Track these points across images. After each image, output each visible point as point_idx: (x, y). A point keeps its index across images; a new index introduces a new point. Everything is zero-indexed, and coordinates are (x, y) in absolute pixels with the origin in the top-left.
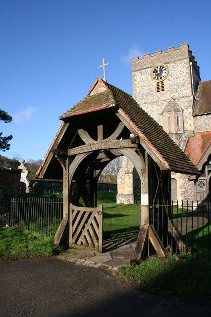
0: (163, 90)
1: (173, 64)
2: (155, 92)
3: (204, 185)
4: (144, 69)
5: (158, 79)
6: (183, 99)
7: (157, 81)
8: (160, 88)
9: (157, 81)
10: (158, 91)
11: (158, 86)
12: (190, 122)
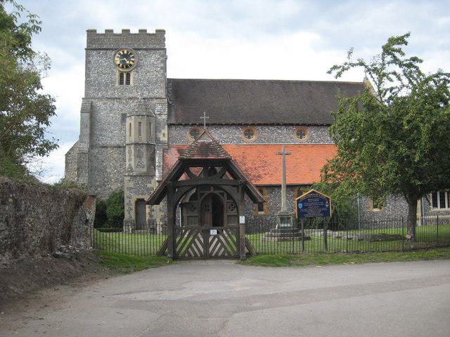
0: (128, 82)
1: (145, 52)
2: (117, 85)
3: (195, 208)
4: (104, 49)
5: (123, 67)
6: (155, 101)
7: (121, 70)
8: (124, 79)
9: (121, 70)
10: (121, 83)
11: (121, 75)
12: (163, 131)
